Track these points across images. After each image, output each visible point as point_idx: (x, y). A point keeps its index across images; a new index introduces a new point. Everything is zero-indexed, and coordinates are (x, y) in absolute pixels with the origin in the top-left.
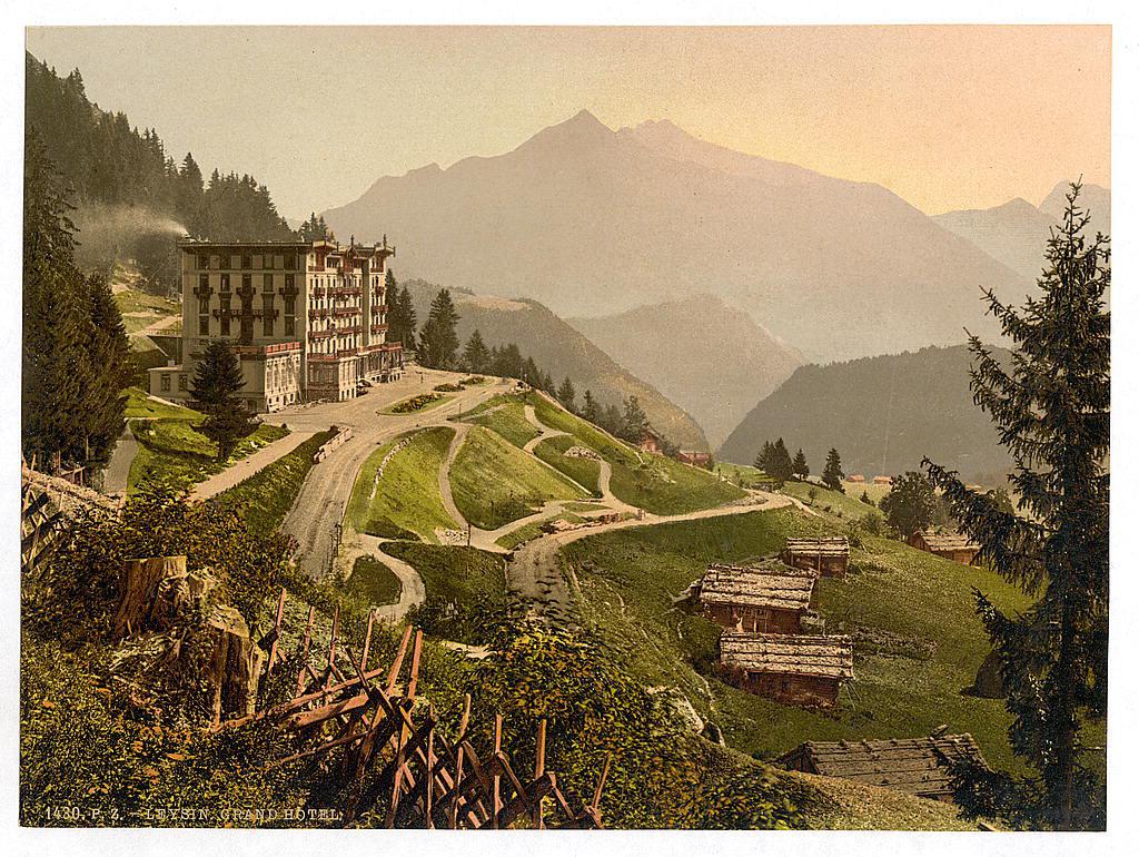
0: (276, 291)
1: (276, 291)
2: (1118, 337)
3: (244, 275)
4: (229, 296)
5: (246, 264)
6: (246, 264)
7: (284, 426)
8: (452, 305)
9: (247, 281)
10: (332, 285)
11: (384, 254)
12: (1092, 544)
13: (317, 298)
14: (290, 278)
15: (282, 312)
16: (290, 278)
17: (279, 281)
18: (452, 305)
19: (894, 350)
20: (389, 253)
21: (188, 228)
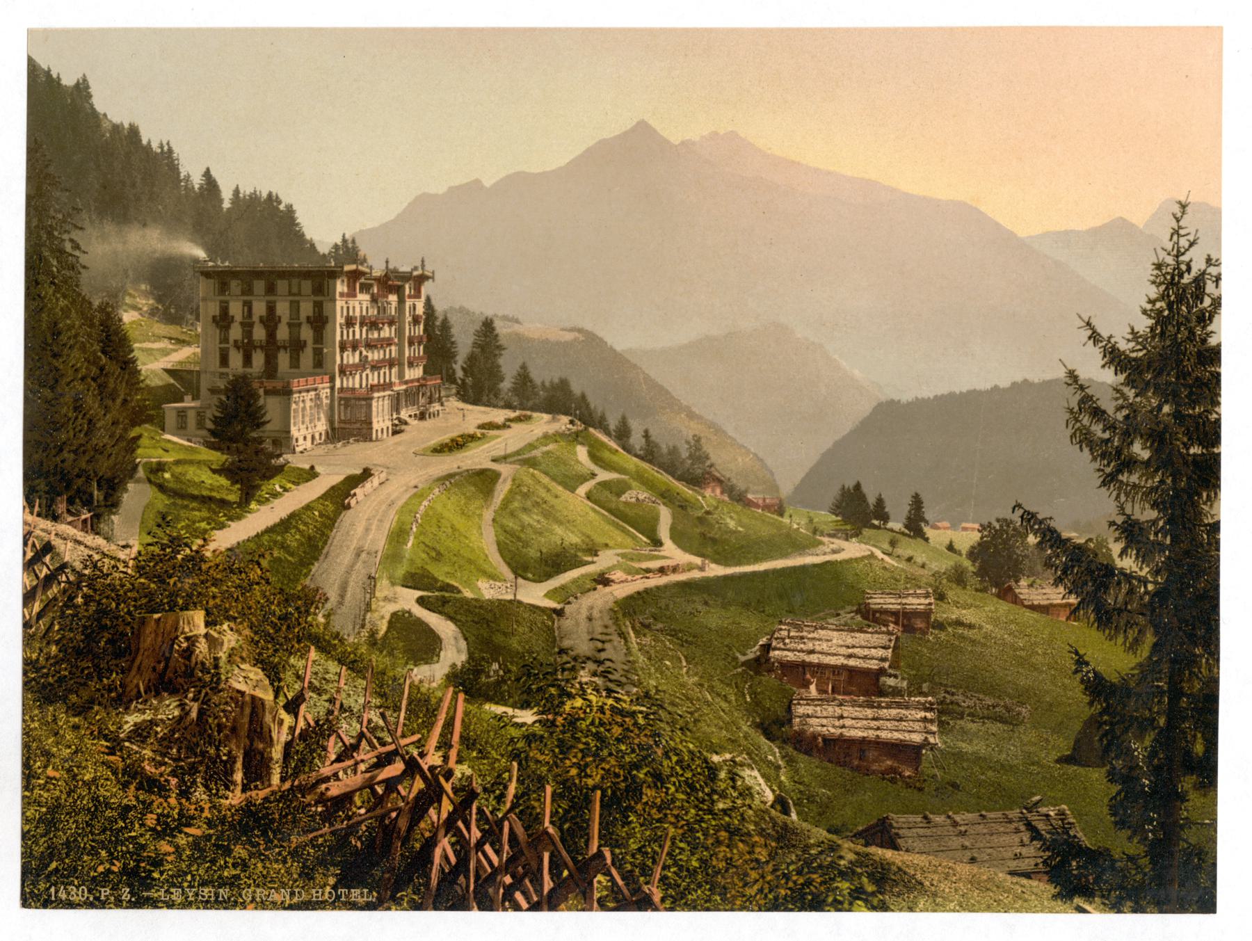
5: (271, 289)
6: (271, 289)
9: (271, 308)
10: (364, 313)
11: (422, 279)
14: (318, 306)
16: (318, 306)
17: (306, 309)
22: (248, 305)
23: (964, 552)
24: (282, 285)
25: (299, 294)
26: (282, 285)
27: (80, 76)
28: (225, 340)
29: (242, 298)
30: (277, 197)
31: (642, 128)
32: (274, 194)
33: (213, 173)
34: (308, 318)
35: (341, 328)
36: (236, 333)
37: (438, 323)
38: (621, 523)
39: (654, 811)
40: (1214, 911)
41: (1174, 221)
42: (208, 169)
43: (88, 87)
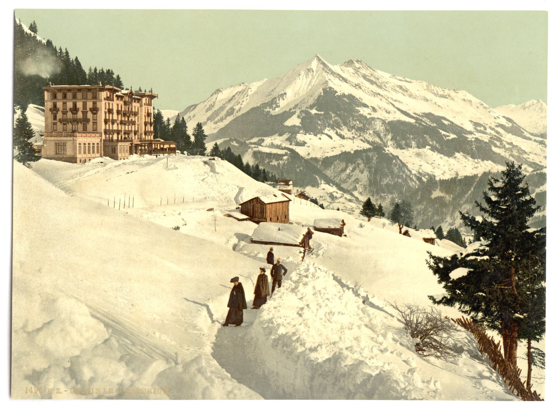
0: (88, 109)
1: (88, 109)
2: (81, 63)
3: (83, 102)
4: (87, 112)
5: (74, 97)
6: (74, 97)
7: (157, 157)
8: (203, 130)
9: (75, 105)
10: (120, 109)
11: (152, 97)
12: (295, 396)
13: (109, 113)
14: (94, 103)
15: (91, 120)
16: (94, 103)
17: (90, 105)
18: (203, 130)
19: (455, 270)
20: (155, 97)
21: (491, 150)
22: (64, 103)
23: (357, 191)
24: (79, 95)
25: (86, 99)
26: (79, 95)
27: (32, 22)
28: (55, 118)
29: (62, 101)
30: (112, 72)
31: (441, 240)
32: (111, 70)
33: (79, 59)
34: (90, 109)
35: (106, 114)
36: (60, 115)
37: (251, 168)
38: (78, 148)
39: (23, 284)
40: (544, 15)
41: (431, 311)
42: (77, 57)
43: (36, 27)
